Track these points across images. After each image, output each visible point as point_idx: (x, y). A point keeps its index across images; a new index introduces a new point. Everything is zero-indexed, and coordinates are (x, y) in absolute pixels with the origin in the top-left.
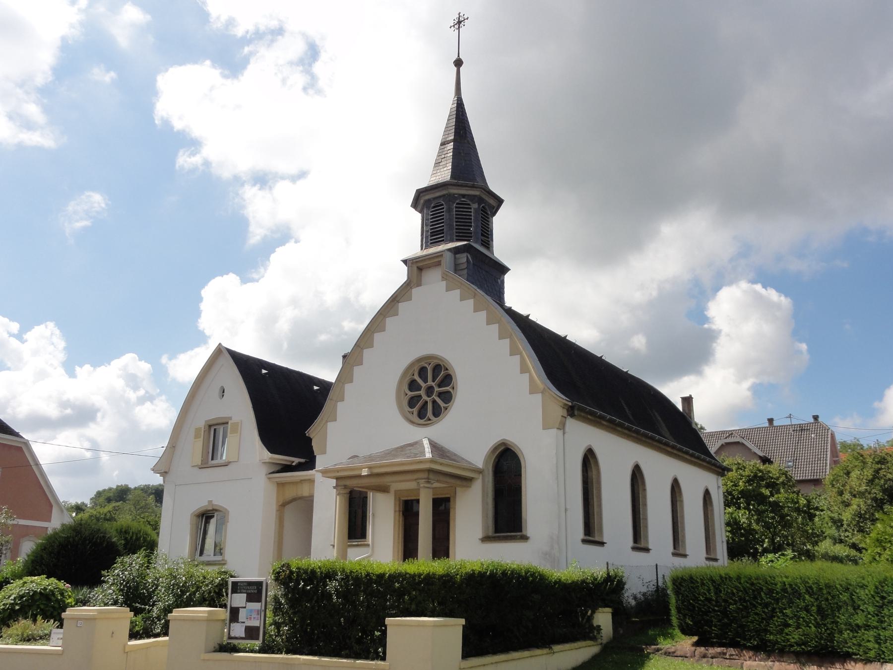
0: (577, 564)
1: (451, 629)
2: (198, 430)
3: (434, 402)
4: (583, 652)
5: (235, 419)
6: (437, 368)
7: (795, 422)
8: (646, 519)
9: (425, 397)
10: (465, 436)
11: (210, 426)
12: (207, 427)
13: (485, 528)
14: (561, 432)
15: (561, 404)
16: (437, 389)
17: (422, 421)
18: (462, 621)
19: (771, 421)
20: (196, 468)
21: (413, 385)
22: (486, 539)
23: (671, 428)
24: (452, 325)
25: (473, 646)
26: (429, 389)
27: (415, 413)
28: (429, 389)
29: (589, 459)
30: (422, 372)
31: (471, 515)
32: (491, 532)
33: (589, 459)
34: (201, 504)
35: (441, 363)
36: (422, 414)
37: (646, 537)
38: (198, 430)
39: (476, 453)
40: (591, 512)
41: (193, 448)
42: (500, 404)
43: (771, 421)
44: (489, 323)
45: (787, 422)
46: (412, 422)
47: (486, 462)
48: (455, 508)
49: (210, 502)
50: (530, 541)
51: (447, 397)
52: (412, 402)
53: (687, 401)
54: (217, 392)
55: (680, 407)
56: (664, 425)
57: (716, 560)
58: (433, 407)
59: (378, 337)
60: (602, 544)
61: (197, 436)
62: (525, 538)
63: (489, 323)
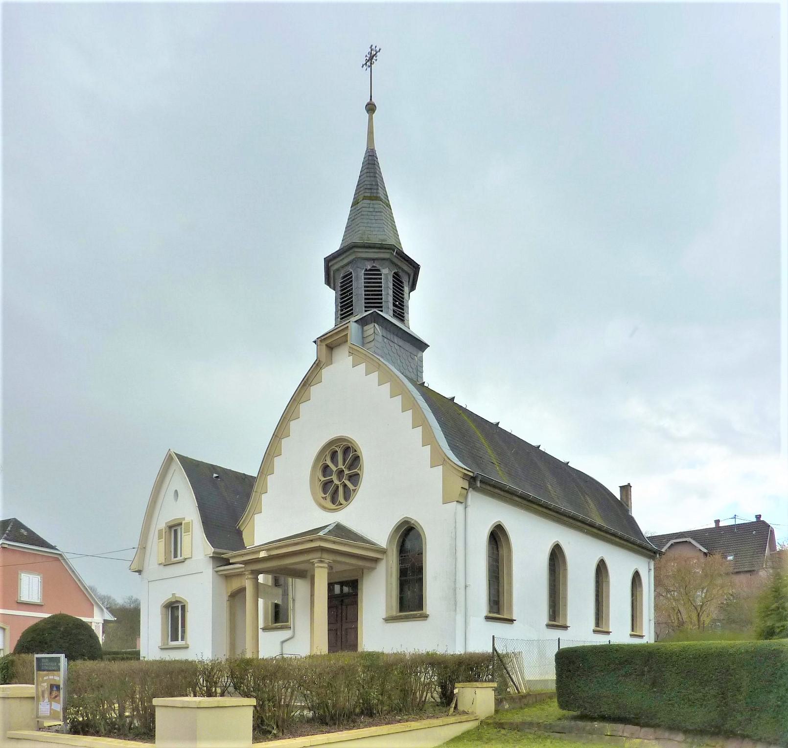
0: (478, 638)
1: (242, 711)
2: (160, 531)
3: (345, 486)
4: (448, 728)
5: (187, 520)
6: (347, 450)
7: (739, 522)
8: (565, 598)
9: (336, 482)
10: (370, 517)
11: (170, 527)
12: (167, 529)
13: (388, 607)
14: (460, 507)
15: (461, 475)
16: (346, 472)
17: (333, 507)
18: (253, 701)
19: (717, 522)
20: (162, 567)
21: (326, 469)
22: (389, 619)
23: (604, 514)
24: (361, 402)
25: (262, 729)
26: (340, 469)
27: (329, 499)
28: (340, 469)
29: (498, 537)
30: (334, 455)
31: (377, 596)
32: (395, 612)
33: (498, 537)
34: (166, 597)
35: (350, 445)
36: (334, 500)
37: (565, 615)
38: (160, 531)
39: (379, 532)
40: (501, 590)
41: (157, 548)
42: (406, 483)
43: (717, 522)
44: (380, 384)
45: (731, 522)
46: (324, 508)
47: (390, 541)
48: (362, 589)
49: (173, 594)
50: (429, 619)
51: (355, 478)
52: (326, 486)
53: (626, 489)
54: (172, 493)
55: (618, 496)
56: (592, 505)
57: (642, 637)
58: (344, 492)
59: (293, 425)
60: (511, 621)
61: (160, 537)
62: (426, 617)
63: (380, 384)
